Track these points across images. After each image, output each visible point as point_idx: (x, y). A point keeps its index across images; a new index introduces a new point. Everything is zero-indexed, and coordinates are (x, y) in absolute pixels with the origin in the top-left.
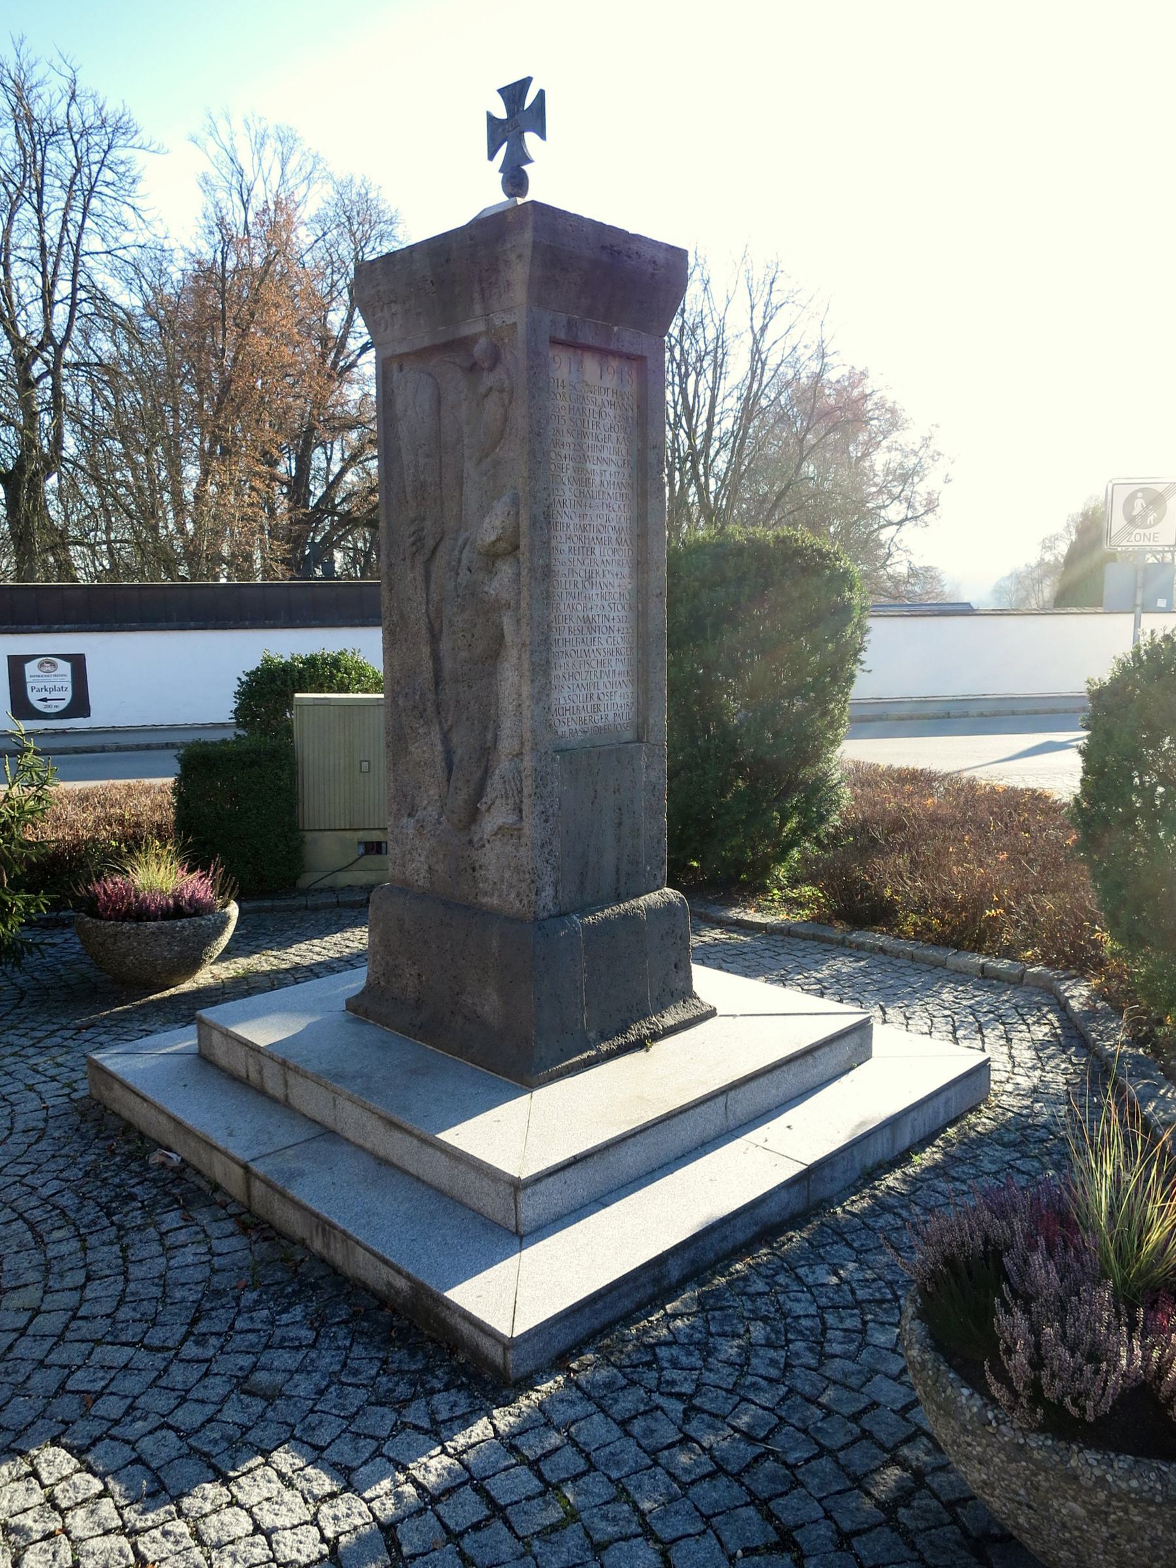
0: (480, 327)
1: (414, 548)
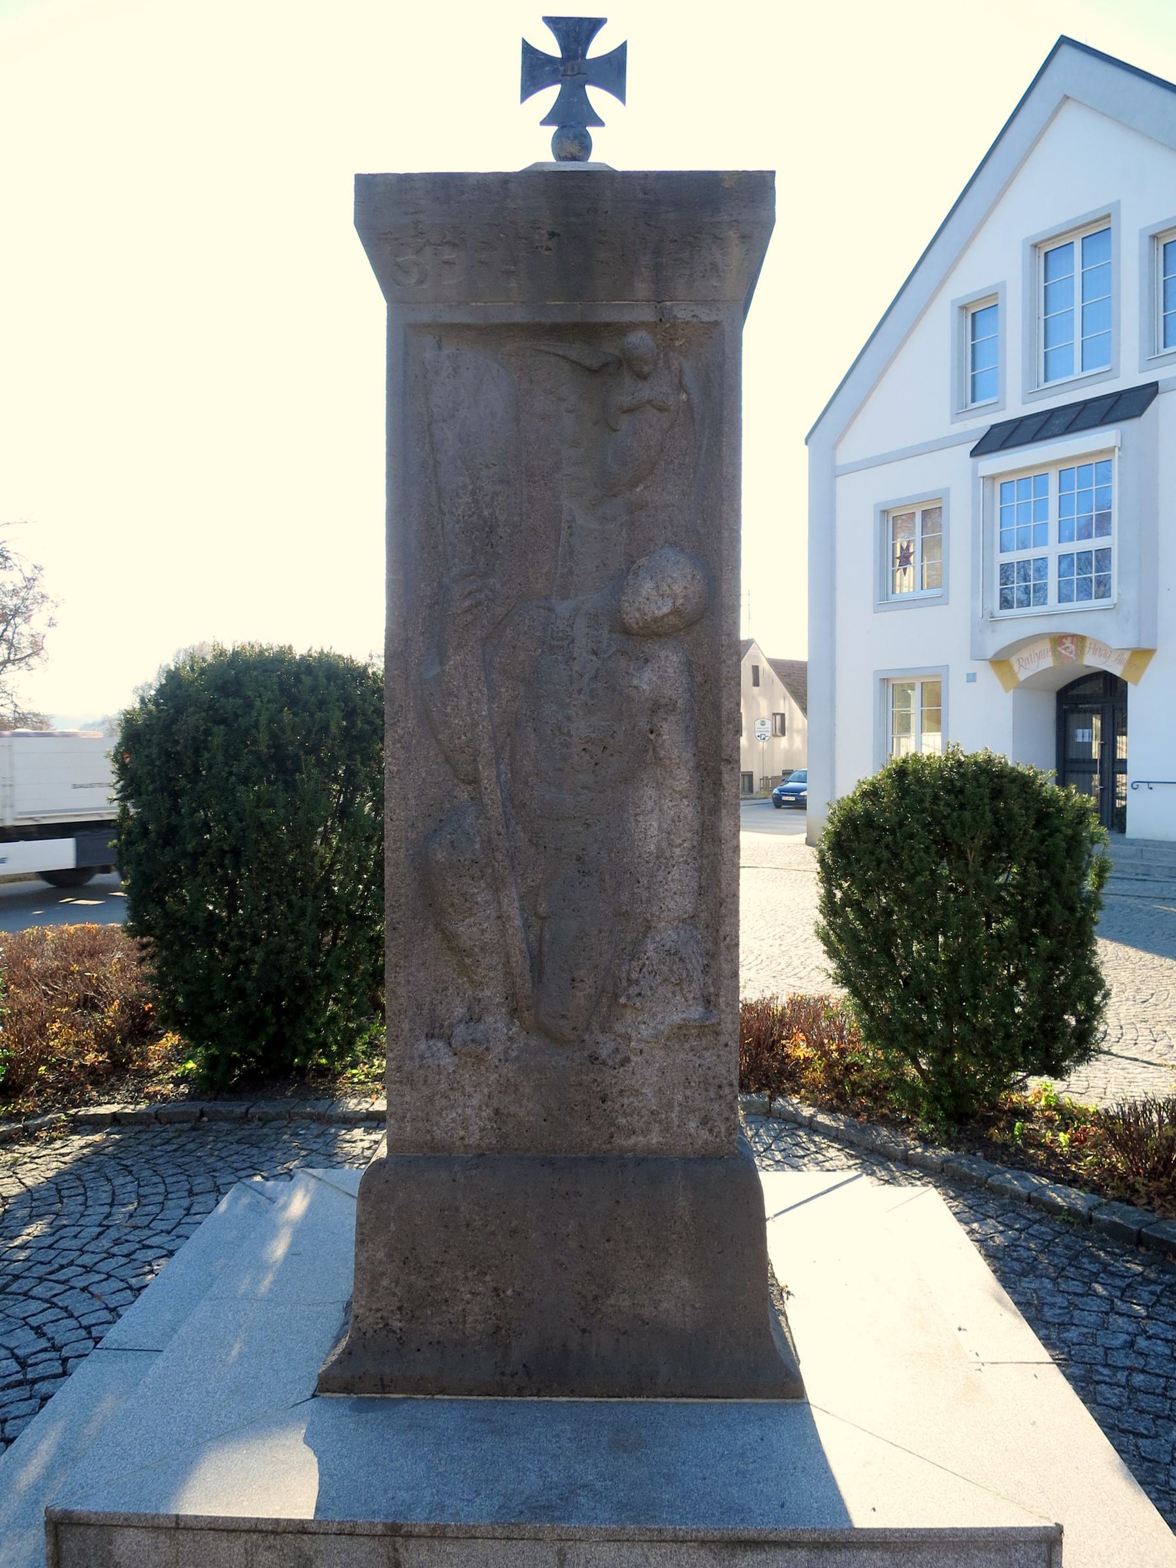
0: (646, 314)
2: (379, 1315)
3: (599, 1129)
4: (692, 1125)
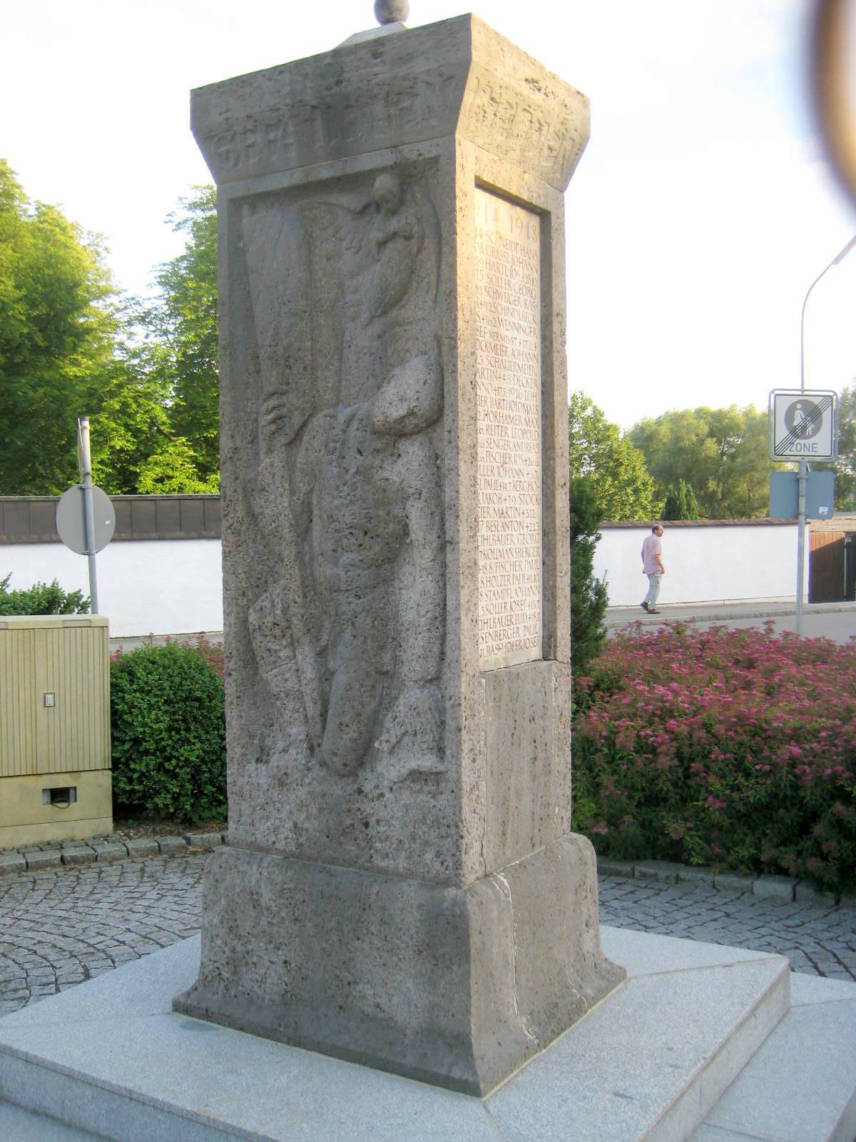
1: (273, 427)
2: (216, 965)
3: (363, 850)
4: (429, 856)
